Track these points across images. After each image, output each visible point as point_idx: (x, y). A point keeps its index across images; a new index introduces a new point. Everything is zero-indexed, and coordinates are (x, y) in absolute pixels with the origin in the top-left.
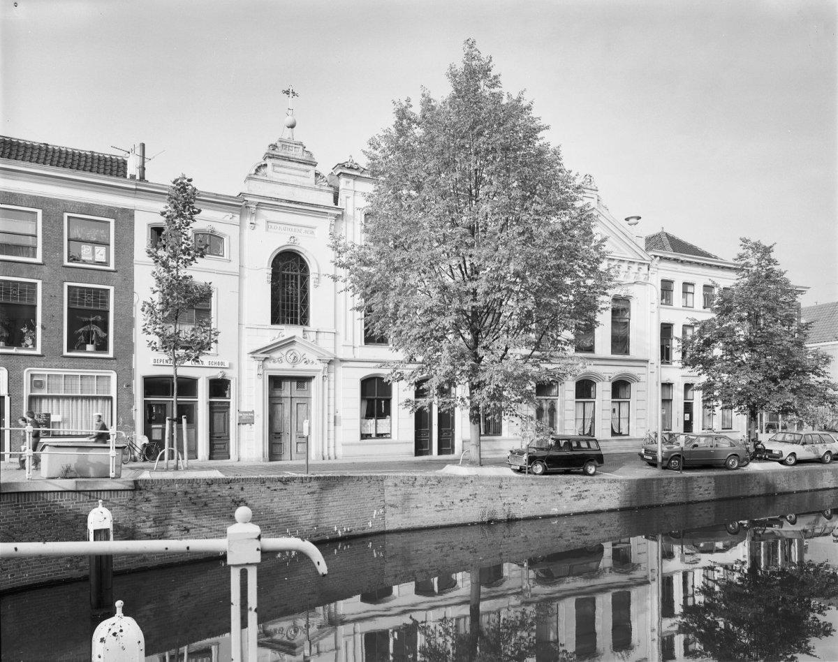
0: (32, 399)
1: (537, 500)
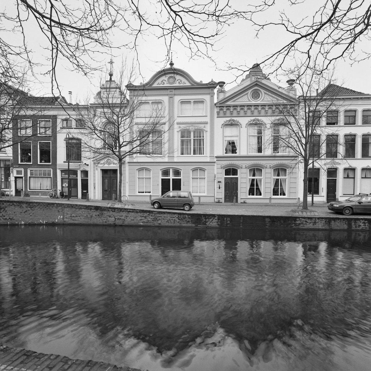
0: (30, 177)
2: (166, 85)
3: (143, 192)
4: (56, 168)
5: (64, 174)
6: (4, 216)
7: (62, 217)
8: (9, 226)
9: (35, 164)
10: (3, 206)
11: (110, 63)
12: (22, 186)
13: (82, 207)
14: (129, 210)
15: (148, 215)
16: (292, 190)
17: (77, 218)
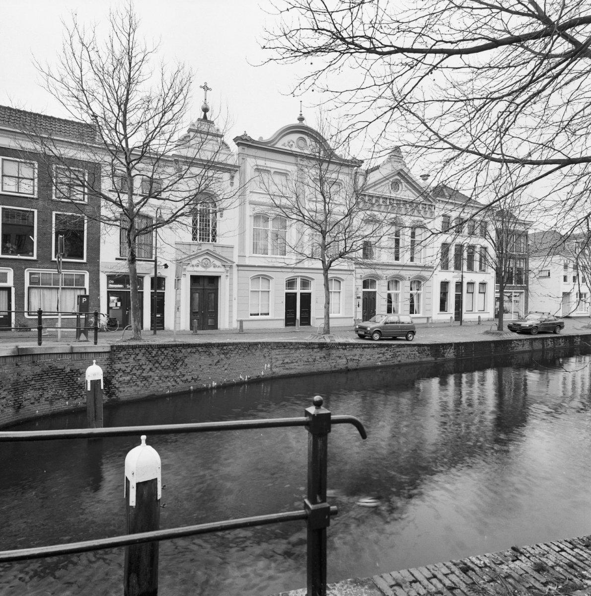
0: (29, 288)
1: (368, 357)
2: (295, 149)
3: (258, 315)
4: (99, 270)
5: (113, 282)
6: (184, 375)
7: (269, 365)
8: (192, 395)
9: (44, 260)
10: (181, 355)
11: (208, 89)
12: (4, 307)
13: (300, 346)
14: (363, 346)
15: (387, 350)
16: (428, 307)
17: (293, 364)
